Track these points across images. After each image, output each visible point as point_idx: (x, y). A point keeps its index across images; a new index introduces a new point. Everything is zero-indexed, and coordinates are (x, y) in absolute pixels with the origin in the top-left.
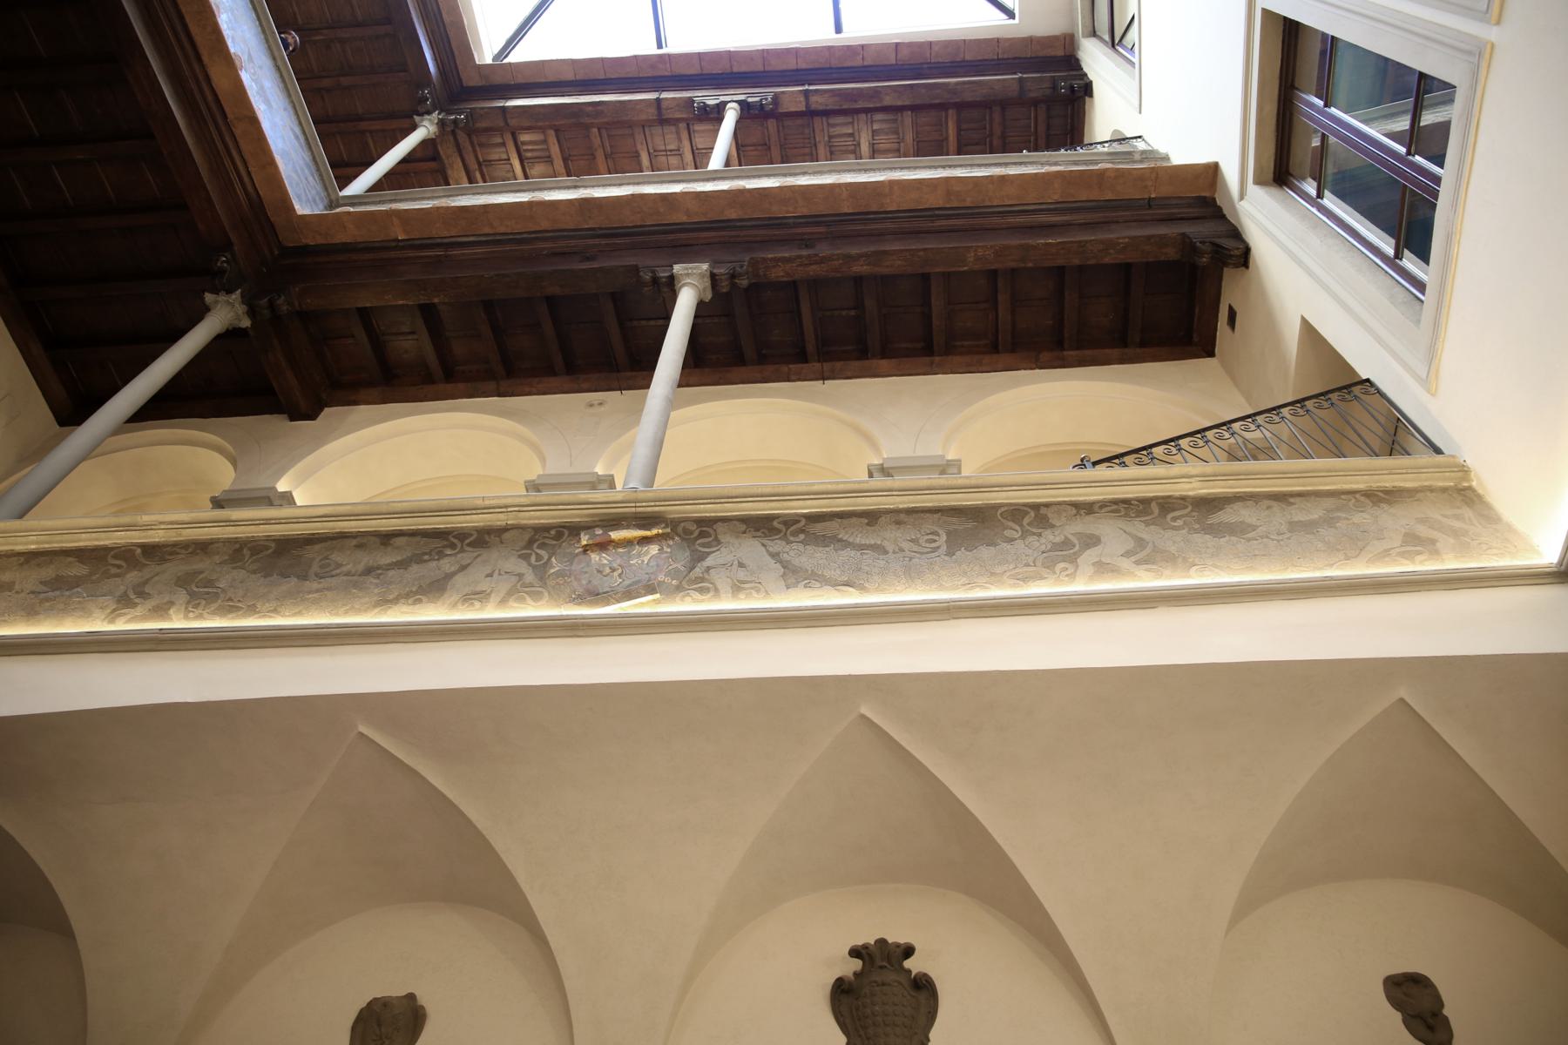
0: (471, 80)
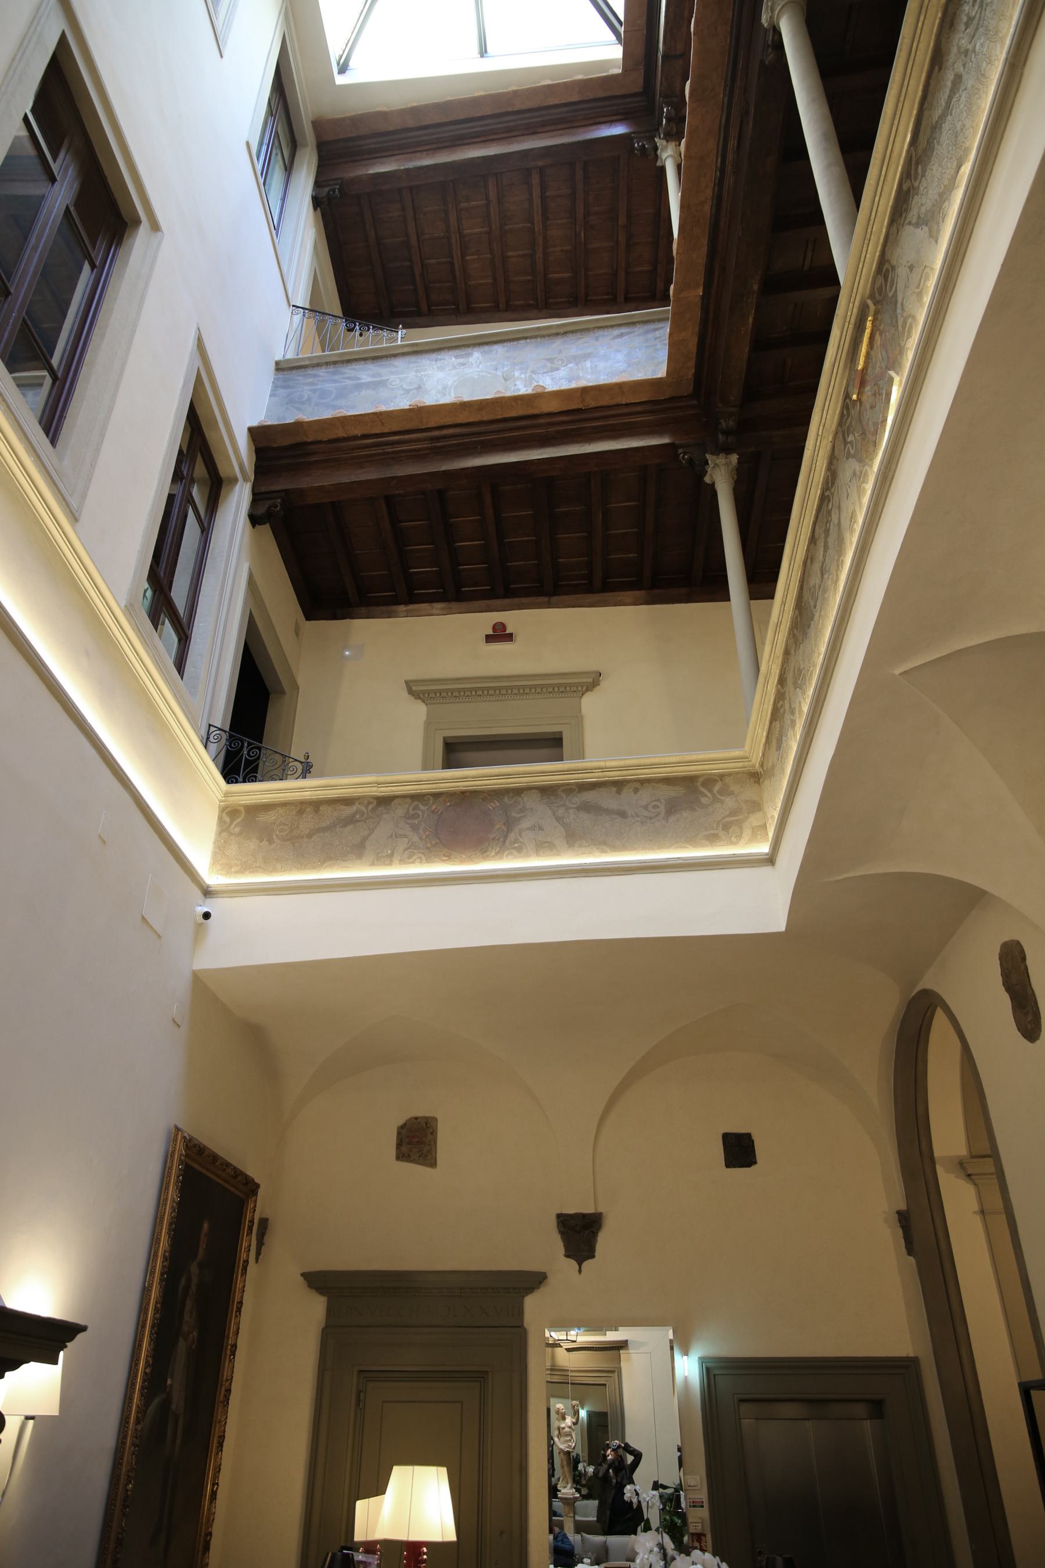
0: (636, 83)
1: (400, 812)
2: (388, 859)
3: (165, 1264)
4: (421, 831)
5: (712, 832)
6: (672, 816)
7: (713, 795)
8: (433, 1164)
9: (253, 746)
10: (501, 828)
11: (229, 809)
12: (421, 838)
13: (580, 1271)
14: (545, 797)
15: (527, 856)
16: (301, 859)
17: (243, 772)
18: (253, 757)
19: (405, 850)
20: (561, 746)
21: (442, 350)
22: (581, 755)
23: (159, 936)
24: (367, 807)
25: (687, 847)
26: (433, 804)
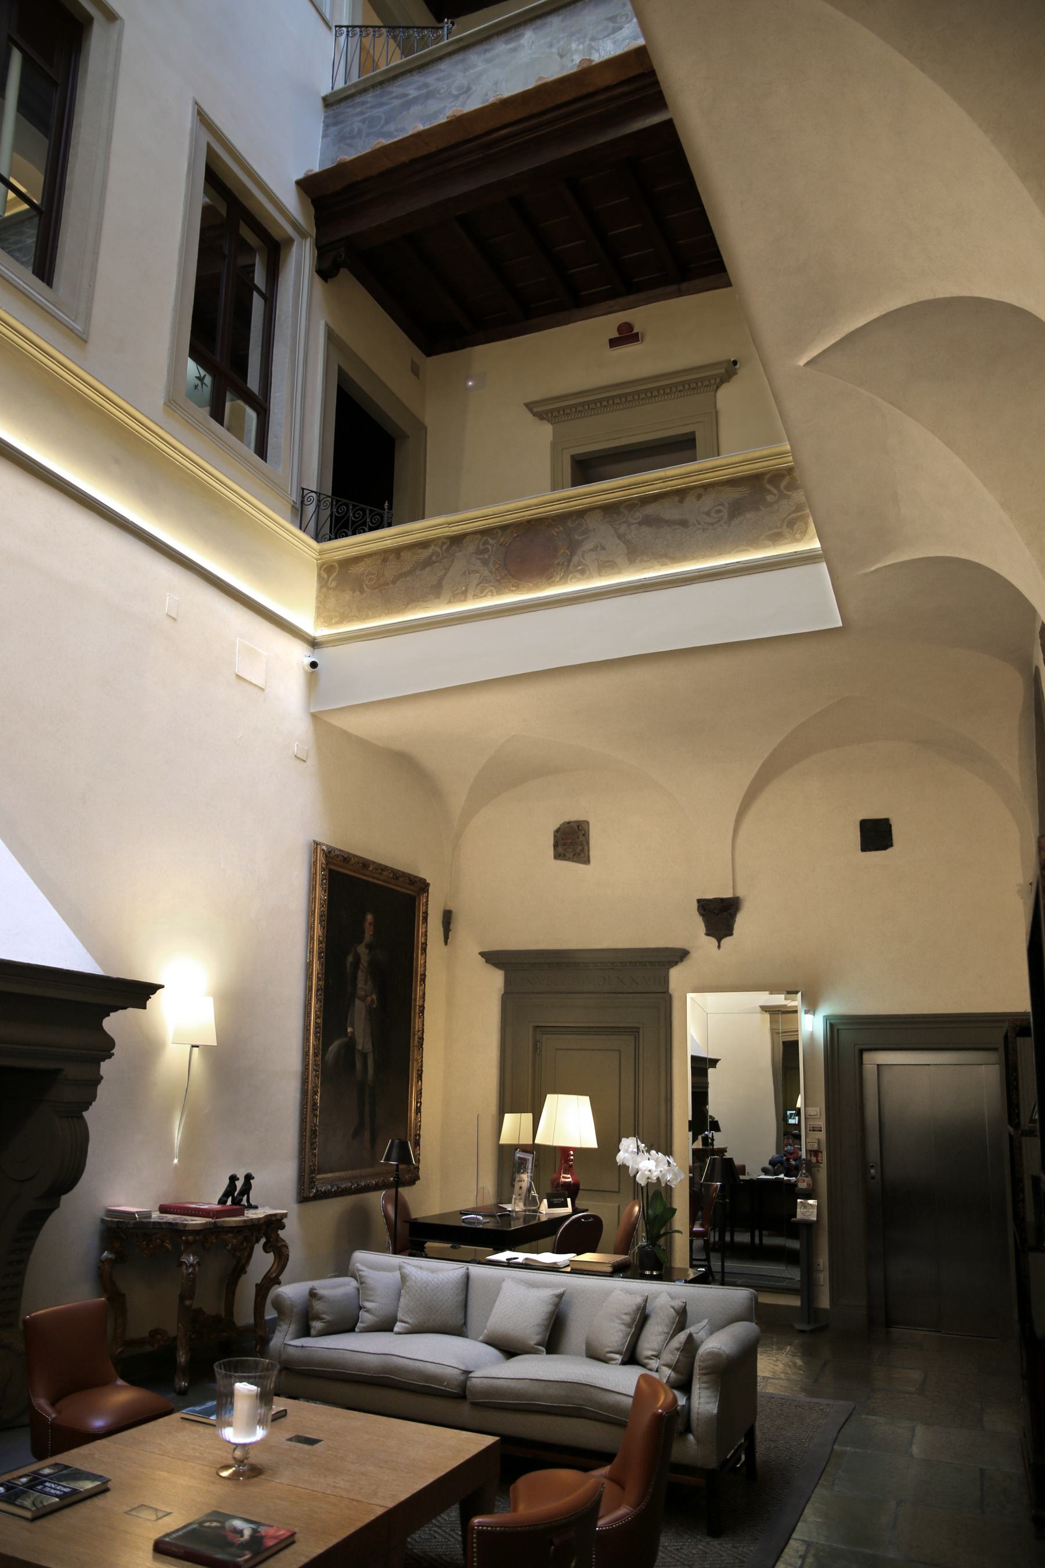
1: (471, 548)
2: (462, 595)
3: (320, 946)
4: (491, 565)
5: (776, 531)
6: (735, 519)
7: (780, 491)
8: (587, 861)
9: (341, 503)
10: (565, 552)
11: (325, 566)
12: (491, 572)
13: (719, 947)
14: (607, 516)
15: (590, 577)
16: (389, 606)
17: (334, 530)
18: (342, 513)
19: (477, 586)
20: (694, 447)
21: (491, 38)
22: (716, 451)
23: (262, 689)
24: (441, 548)
25: (748, 550)
26: (501, 536)
